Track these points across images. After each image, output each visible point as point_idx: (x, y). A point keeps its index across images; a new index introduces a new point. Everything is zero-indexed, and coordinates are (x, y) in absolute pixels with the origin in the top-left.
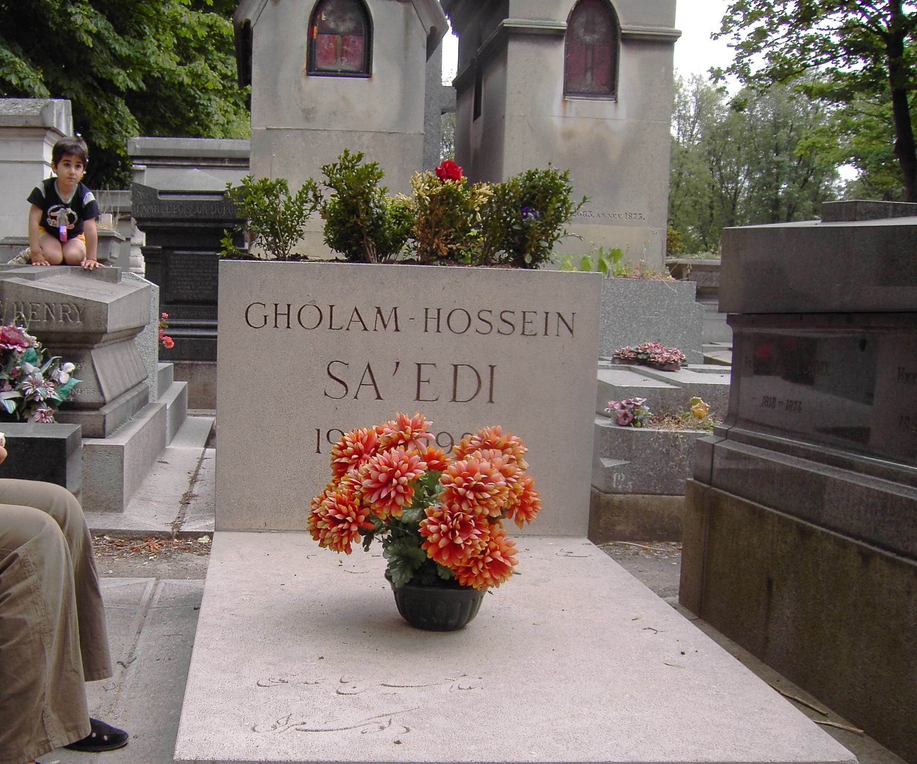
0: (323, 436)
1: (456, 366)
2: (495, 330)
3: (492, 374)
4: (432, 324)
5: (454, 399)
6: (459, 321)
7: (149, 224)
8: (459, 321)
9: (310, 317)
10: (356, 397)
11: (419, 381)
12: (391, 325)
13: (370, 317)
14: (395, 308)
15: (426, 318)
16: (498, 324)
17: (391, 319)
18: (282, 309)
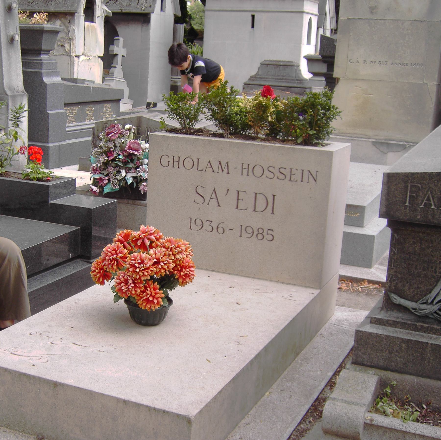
0: (193, 221)
1: (256, 194)
2: (276, 177)
3: (274, 199)
4: (245, 171)
5: (237, 208)
6: (258, 171)
7: (327, 59)
8: (258, 171)
9: (188, 163)
10: (208, 204)
11: (238, 200)
12: (226, 171)
13: (216, 166)
14: (228, 162)
15: (242, 168)
16: (277, 174)
17: (225, 167)
18: (176, 159)
